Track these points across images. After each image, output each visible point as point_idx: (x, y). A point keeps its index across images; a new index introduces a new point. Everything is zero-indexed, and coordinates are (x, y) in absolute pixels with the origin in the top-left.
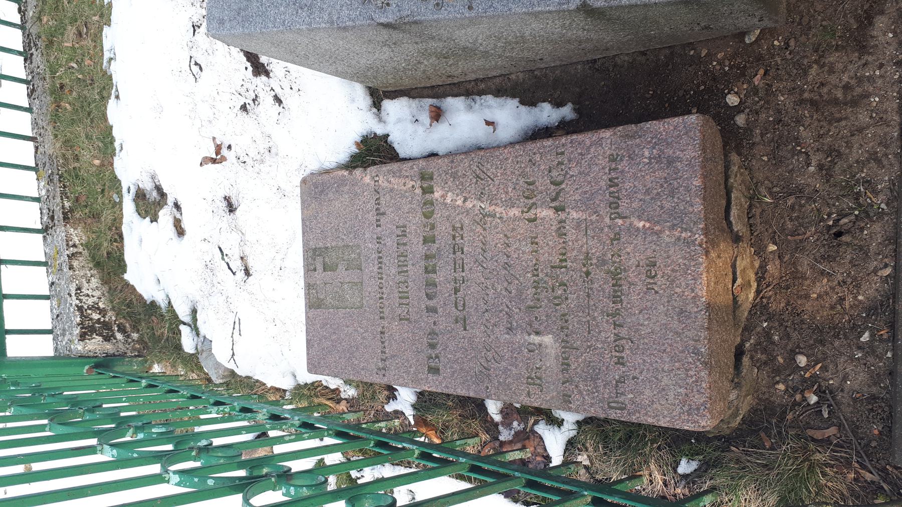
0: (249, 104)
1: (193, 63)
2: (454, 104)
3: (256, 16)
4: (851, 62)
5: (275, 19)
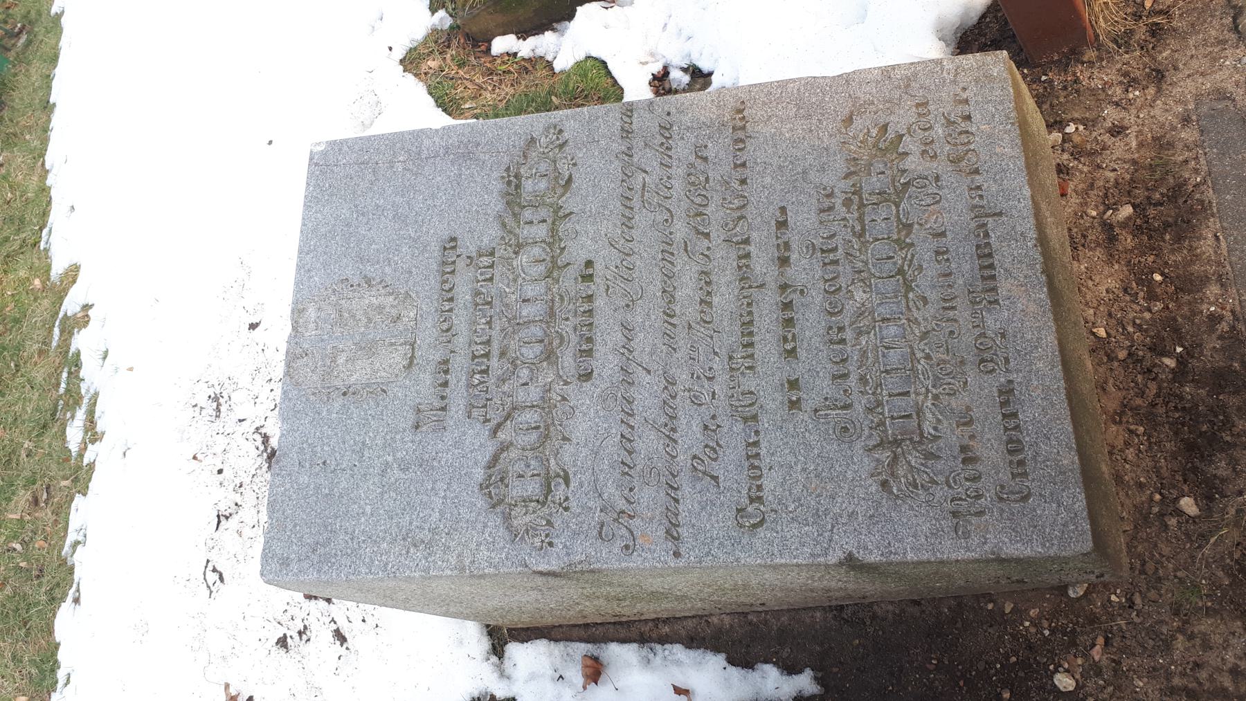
0: (291, 637)
1: (210, 567)
2: (620, 655)
3: (342, 556)
4: (1233, 634)
5: (372, 561)
